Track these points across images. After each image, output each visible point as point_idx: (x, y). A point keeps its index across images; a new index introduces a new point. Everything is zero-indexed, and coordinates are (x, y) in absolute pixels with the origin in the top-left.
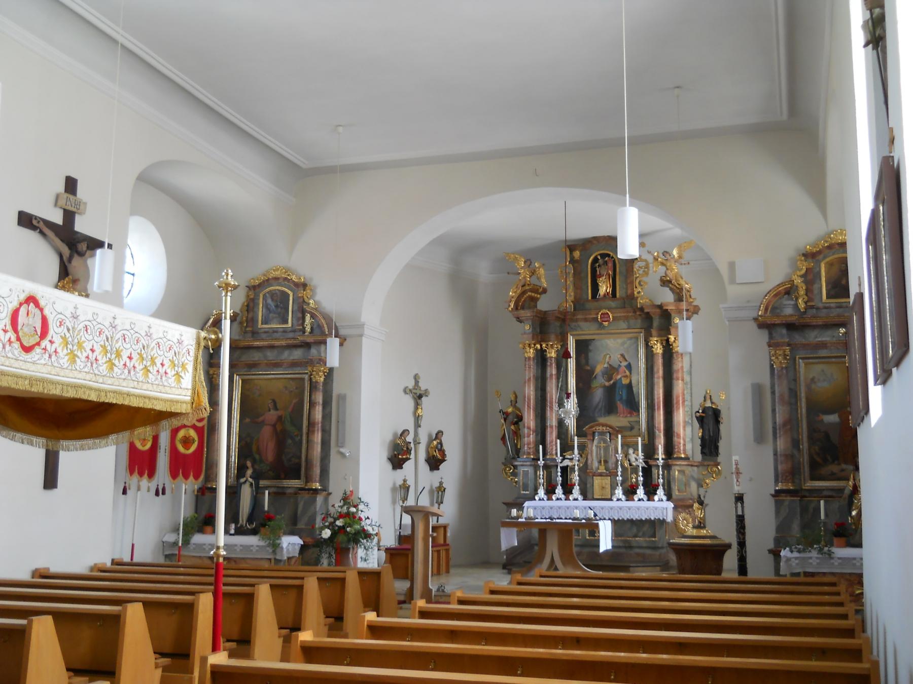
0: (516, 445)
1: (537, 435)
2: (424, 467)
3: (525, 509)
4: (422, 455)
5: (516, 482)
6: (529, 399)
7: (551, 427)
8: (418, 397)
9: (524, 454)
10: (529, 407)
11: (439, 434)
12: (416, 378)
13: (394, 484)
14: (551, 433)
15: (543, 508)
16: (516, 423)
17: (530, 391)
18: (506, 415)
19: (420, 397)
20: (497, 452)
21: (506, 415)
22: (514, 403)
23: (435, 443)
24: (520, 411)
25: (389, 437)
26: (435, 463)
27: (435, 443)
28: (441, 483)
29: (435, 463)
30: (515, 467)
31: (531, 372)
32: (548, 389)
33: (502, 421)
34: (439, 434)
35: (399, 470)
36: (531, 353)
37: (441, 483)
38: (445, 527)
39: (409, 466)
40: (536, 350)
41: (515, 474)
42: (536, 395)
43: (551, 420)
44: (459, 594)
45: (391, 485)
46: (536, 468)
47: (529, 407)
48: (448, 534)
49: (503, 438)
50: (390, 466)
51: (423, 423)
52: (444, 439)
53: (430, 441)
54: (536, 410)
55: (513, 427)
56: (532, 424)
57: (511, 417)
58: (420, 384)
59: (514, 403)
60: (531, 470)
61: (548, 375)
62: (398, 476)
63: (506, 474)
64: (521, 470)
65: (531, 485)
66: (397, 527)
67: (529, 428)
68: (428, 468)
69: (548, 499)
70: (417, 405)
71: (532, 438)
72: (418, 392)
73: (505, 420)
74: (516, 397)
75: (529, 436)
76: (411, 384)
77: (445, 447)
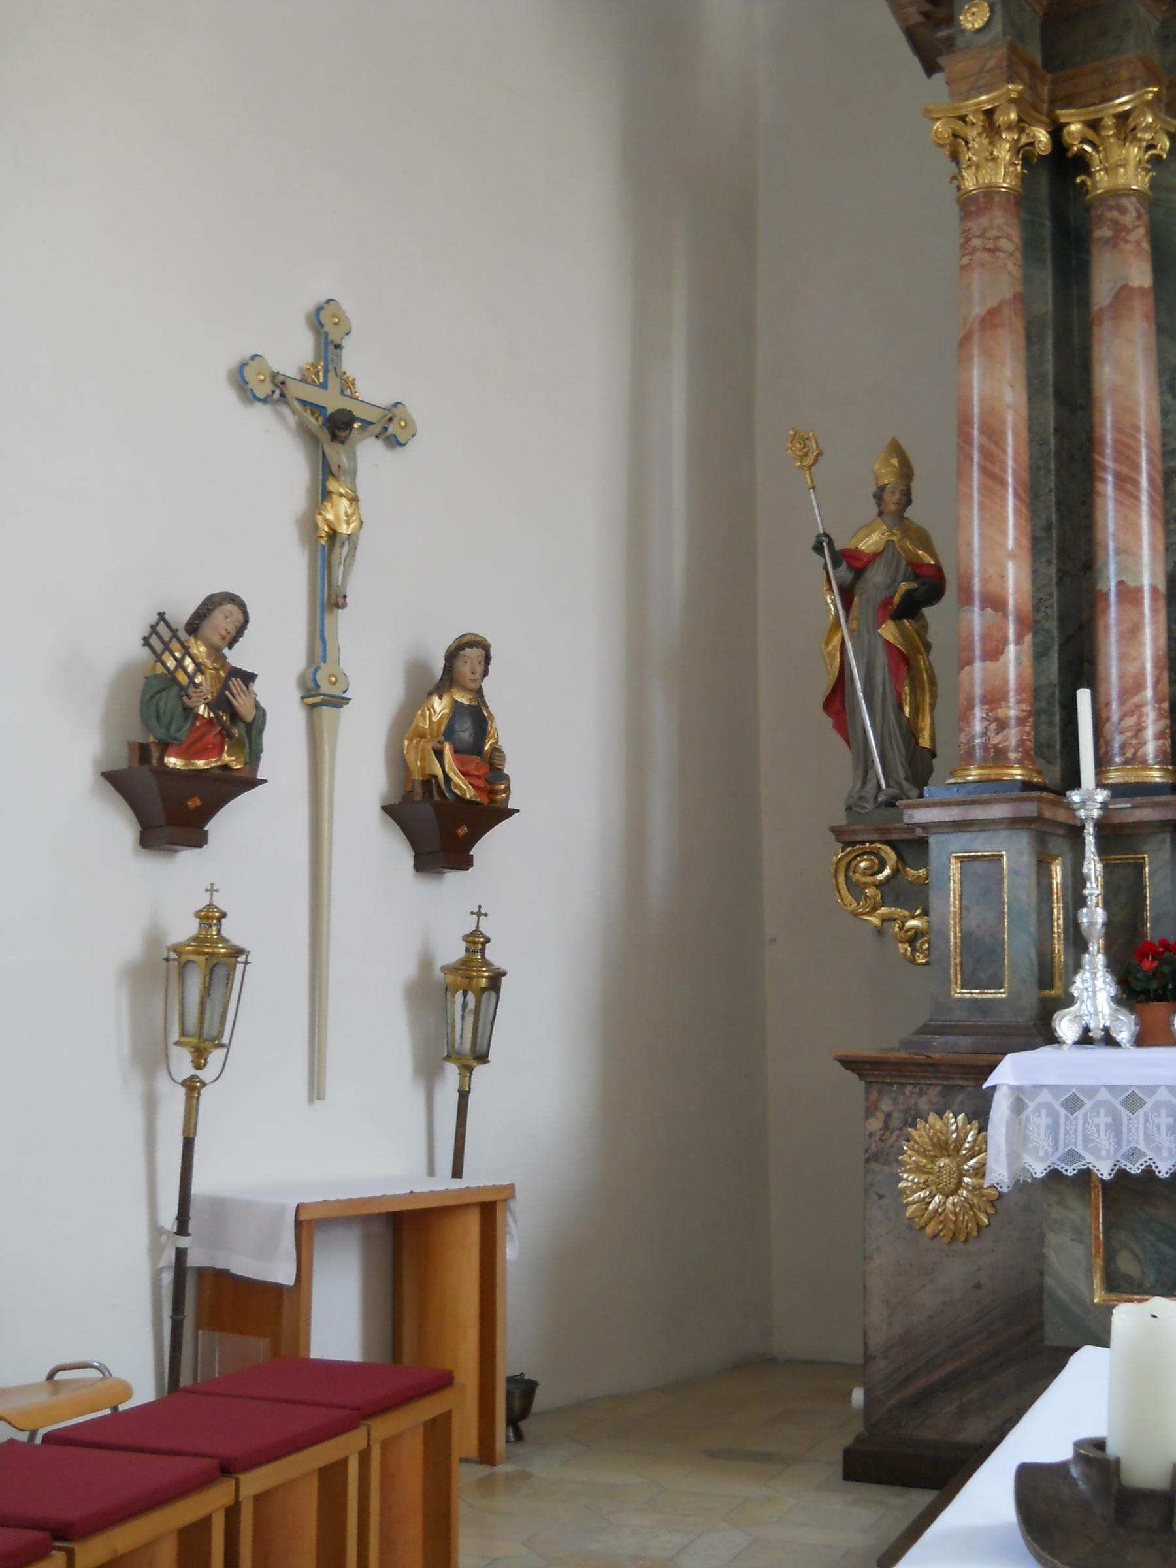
0: (910, 733)
1: (1039, 655)
2: (370, 847)
3: (1001, 1108)
4: (363, 777)
5: (914, 938)
6: (993, 433)
7: (1130, 595)
8: (334, 429)
9: (968, 757)
10: (993, 478)
11: (466, 659)
12: (327, 330)
13: (426, 964)
14: (1132, 632)
15: (1133, 1102)
16: (909, 609)
17: (1000, 386)
18: (852, 566)
19: (340, 425)
20: (808, 778)
21: (852, 566)
22: (896, 501)
23: (440, 706)
24: (924, 541)
25: (121, 645)
26: (445, 821)
27: (440, 706)
28: (476, 942)
29: (445, 821)
30: (913, 847)
31: (999, 278)
32: (1105, 375)
33: (832, 602)
34: (466, 659)
35: (187, 856)
36: (997, 169)
37: (476, 942)
38: (490, 1210)
39: (254, 836)
40: (1025, 153)
41: (909, 894)
42: (1033, 422)
43: (1127, 552)
44: (1121, 172)
45: (407, 969)
46: (1056, 835)
47: (993, 478)
48: (511, 1251)
49: (837, 700)
50: (118, 827)
51: (361, 582)
52: (498, 692)
53: (422, 686)
54: (1032, 496)
55: (888, 631)
56: (1015, 580)
57: (877, 576)
58: (351, 362)
59: (896, 501)
60: (1013, 854)
61: (1102, 291)
62: (176, 888)
63: (856, 889)
64: (948, 864)
65: (1017, 951)
66: (168, 1216)
67: (994, 602)
68: (405, 856)
69: (1141, 1040)
70: (326, 477)
71: (1014, 661)
72: (332, 402)
73: (847, 596)
74: (906, 472)
75: (994, 652)
76: (292, 353)
77: (508, 732)
